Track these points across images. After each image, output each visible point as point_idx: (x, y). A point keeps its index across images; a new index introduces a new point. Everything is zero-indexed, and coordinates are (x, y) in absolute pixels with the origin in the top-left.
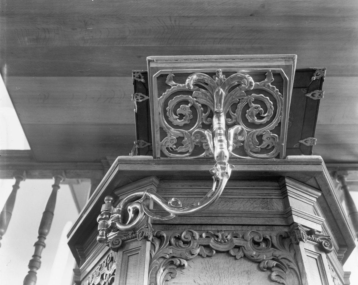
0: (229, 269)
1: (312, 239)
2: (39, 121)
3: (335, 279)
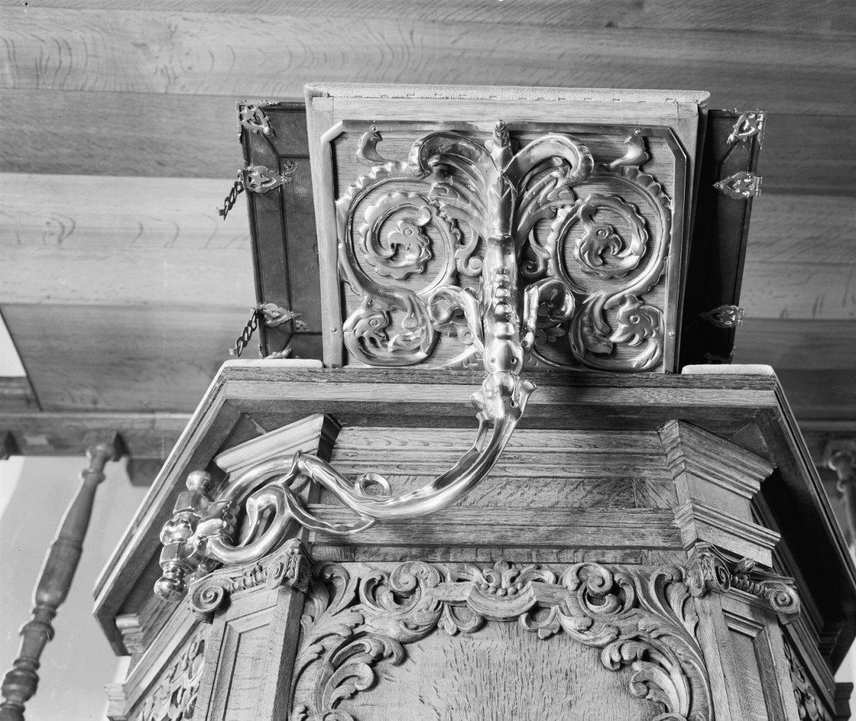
0: (520, 666)
1: (744, 583)
2: (49, 297)
3: (809, 698)
